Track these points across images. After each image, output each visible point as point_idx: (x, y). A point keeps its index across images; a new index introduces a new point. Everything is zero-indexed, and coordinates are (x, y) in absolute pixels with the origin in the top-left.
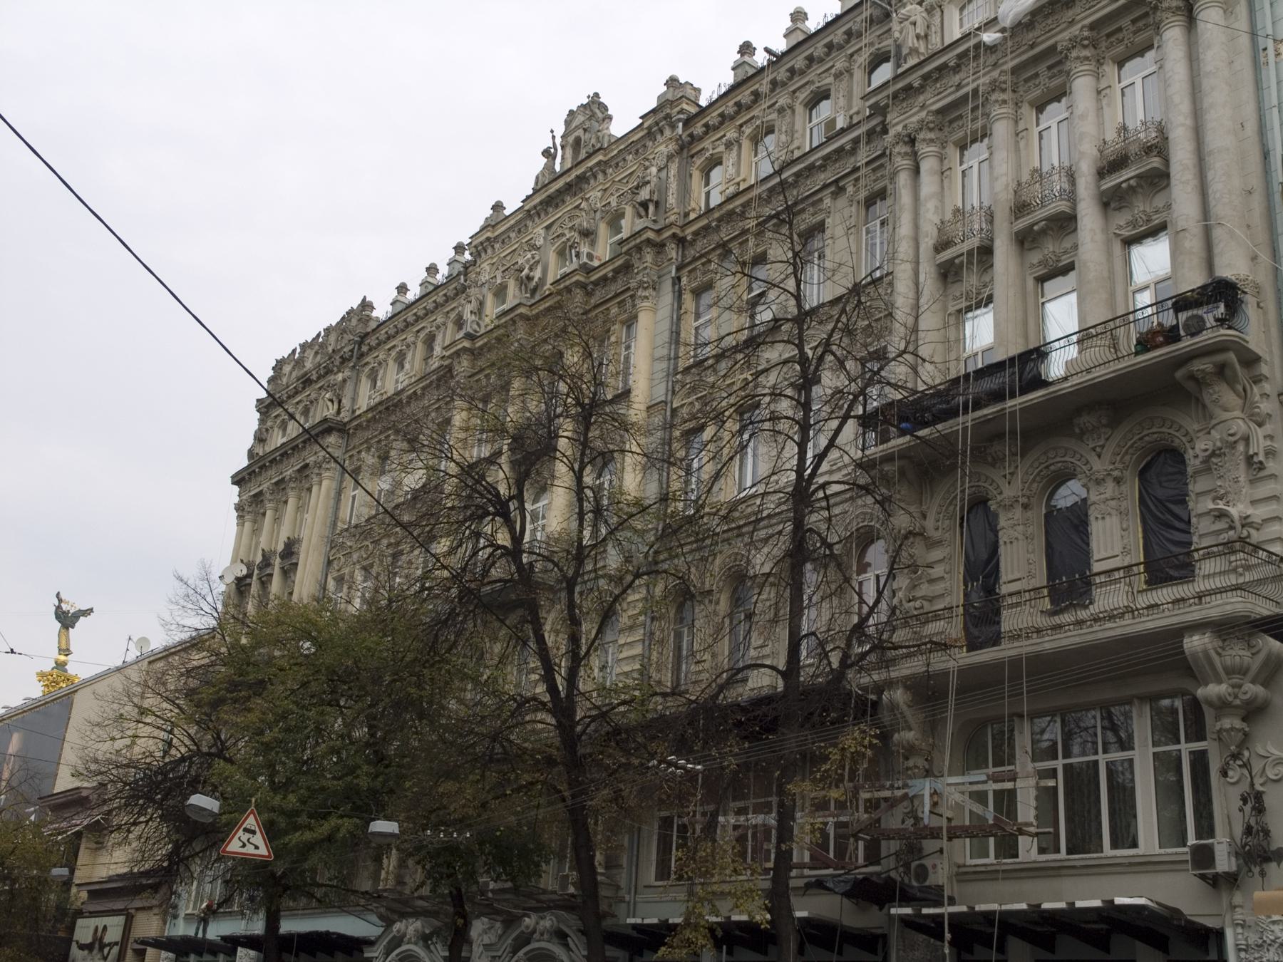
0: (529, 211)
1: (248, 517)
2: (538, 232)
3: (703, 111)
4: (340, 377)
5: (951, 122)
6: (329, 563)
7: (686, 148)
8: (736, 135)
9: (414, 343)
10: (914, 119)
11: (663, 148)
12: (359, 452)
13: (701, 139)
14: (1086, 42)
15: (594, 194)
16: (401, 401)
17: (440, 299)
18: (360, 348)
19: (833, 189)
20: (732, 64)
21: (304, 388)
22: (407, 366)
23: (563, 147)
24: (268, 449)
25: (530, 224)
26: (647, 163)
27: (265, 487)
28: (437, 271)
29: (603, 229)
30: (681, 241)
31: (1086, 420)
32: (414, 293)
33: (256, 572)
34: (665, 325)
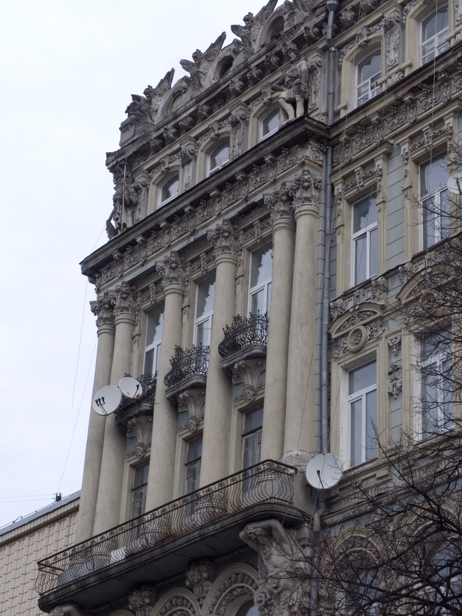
1: (121, 316)
6: (332, 343)
8: (241, 112)
13: (351, 24)
20: (120, 126)
21: (210, 112)
24: (140, 216)
27: (159, 261)
31: (193, 575)
33: (161, 387)
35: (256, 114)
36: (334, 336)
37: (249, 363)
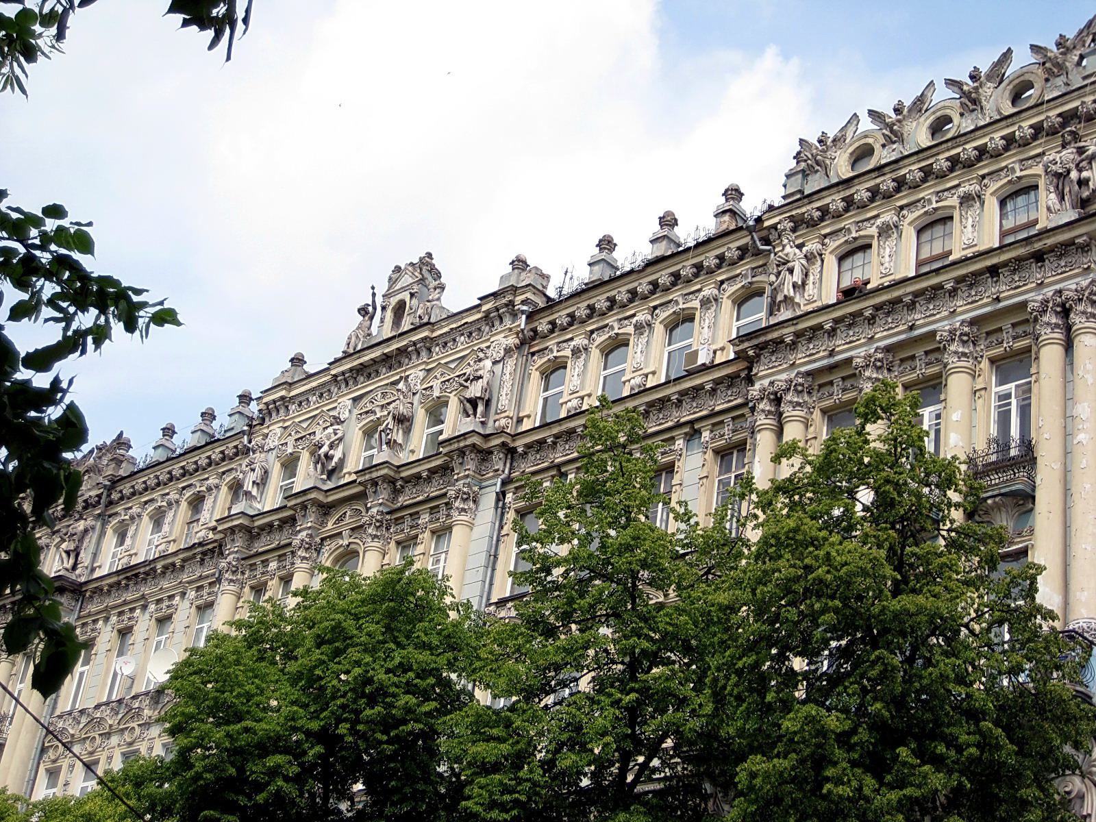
0: (335, 376)
2: (343, 403)
3: (552, 304)
4: (81, 525)
5: (820, 386)
6: (43, 750)
7: (528, 342)
9: (177, 502)
10: (784, 376)
11: (502, 339)
12: (95, 621)
14: (965, 338)
15: (416, 374)
16: (154, 570)
17: (216, 456)
18: (109, 496)
19: (687, 430)
22: (166, 528)
23: (384, 308)
25: (334, 390)
26: (481, 355)
28: (214, 418)
29: (421, 417)
30: (510, 452)
32: (184, 438)
34: (484, 545)
35: (912, 222)
36: (46, 745)
37: (1007, 500)
